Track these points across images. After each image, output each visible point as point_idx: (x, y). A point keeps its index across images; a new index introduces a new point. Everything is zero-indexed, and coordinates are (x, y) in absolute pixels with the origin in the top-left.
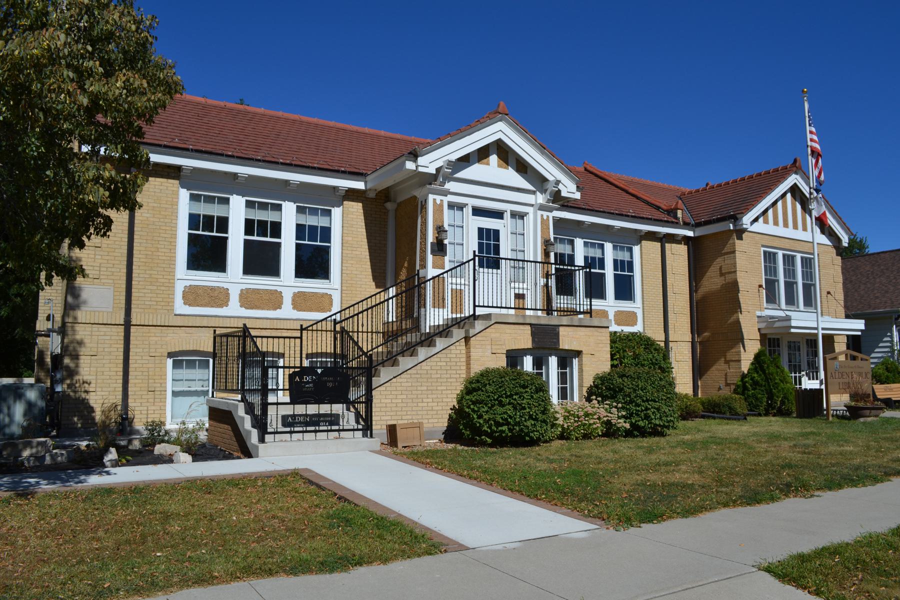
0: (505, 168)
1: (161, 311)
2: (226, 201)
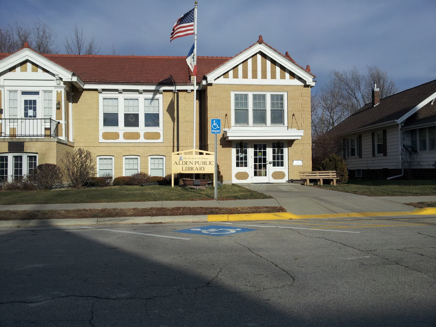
0: (294, 79)
1: (189, 142)
2: (57, 85)
